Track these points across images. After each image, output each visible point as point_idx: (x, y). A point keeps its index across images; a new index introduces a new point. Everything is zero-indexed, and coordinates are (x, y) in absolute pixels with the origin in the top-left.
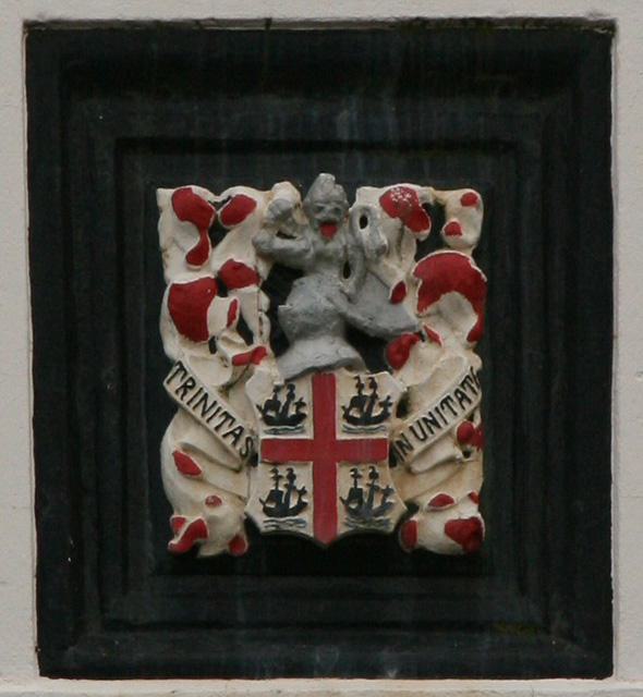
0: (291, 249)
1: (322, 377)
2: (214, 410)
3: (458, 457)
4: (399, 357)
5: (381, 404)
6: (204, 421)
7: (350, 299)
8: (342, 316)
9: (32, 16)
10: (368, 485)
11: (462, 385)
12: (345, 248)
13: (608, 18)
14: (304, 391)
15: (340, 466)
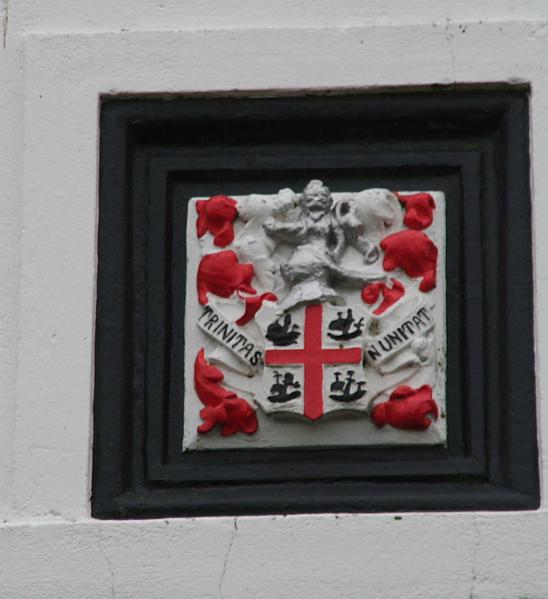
0: (290, 228)
1: (313, 307)
2: (232, 334)
3: (416, 361)
4: (371, 297)
5: (355, 325)
6: (224, 342)
7: (333, 259)
8: (326, 268)
9: (106, 90)
10: (347, 379)
11: (418, 313)
12: (331, 227)
13: (524, 81)
14: (299, 319)
15: (326, 367)
